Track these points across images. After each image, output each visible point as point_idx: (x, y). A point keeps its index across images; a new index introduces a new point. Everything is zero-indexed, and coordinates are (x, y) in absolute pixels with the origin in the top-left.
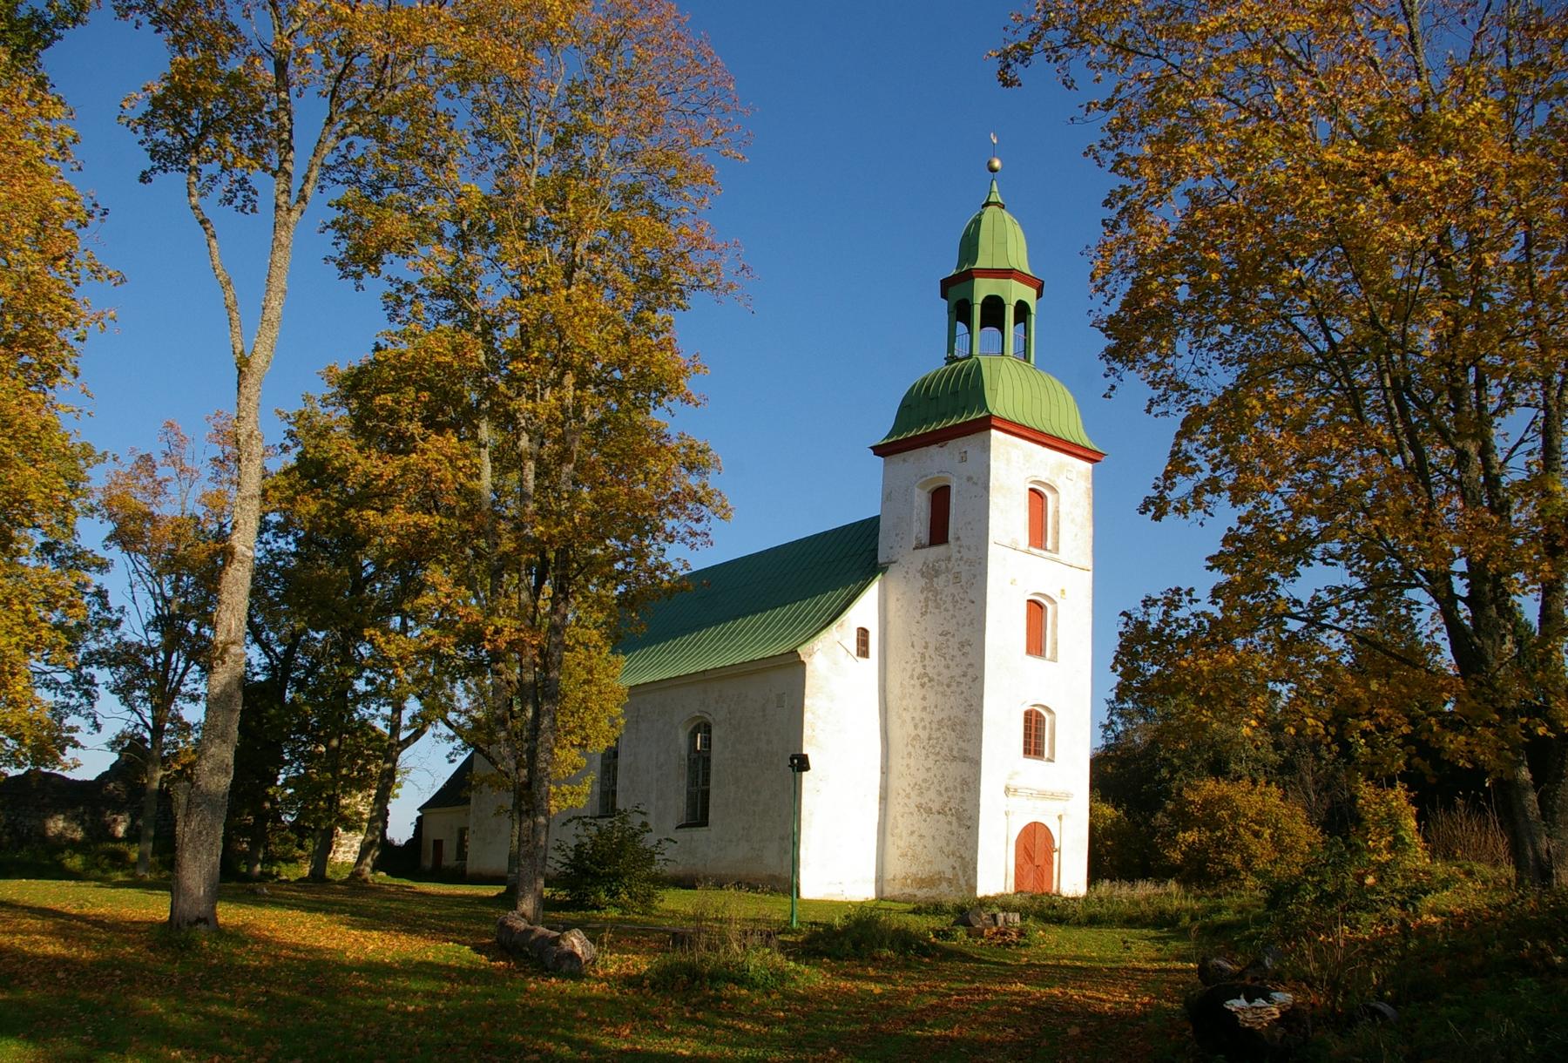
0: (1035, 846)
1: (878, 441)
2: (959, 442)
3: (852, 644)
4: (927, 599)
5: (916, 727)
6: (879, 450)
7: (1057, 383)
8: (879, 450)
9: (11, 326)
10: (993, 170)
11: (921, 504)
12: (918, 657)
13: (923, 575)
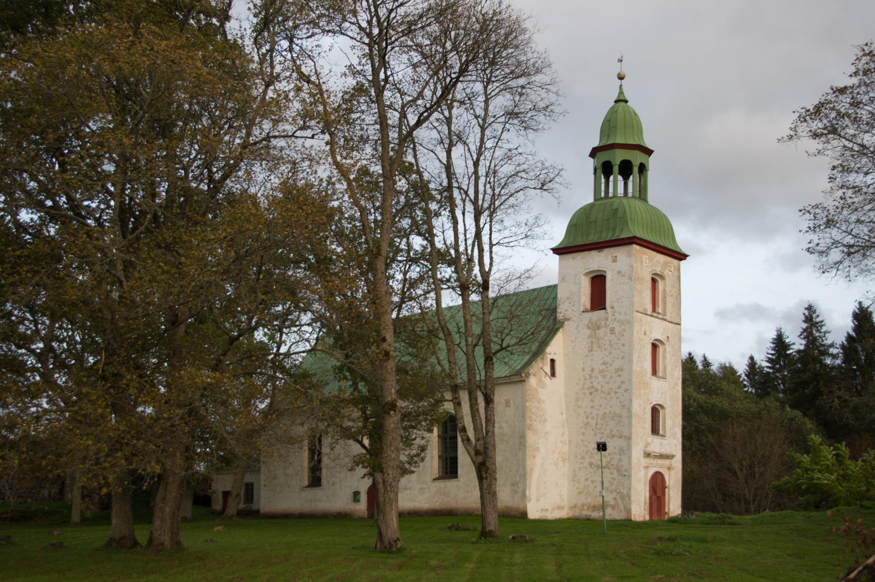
0: (657, 484)
1: (555, 243)
2: (612, 250)
3: (548, 369)
4: (592, 342)
5: (587, 417)
6: (556, 251)
8: (556, 251)
11: (585, 286)
12: (587, 377)
13: (589, 328)
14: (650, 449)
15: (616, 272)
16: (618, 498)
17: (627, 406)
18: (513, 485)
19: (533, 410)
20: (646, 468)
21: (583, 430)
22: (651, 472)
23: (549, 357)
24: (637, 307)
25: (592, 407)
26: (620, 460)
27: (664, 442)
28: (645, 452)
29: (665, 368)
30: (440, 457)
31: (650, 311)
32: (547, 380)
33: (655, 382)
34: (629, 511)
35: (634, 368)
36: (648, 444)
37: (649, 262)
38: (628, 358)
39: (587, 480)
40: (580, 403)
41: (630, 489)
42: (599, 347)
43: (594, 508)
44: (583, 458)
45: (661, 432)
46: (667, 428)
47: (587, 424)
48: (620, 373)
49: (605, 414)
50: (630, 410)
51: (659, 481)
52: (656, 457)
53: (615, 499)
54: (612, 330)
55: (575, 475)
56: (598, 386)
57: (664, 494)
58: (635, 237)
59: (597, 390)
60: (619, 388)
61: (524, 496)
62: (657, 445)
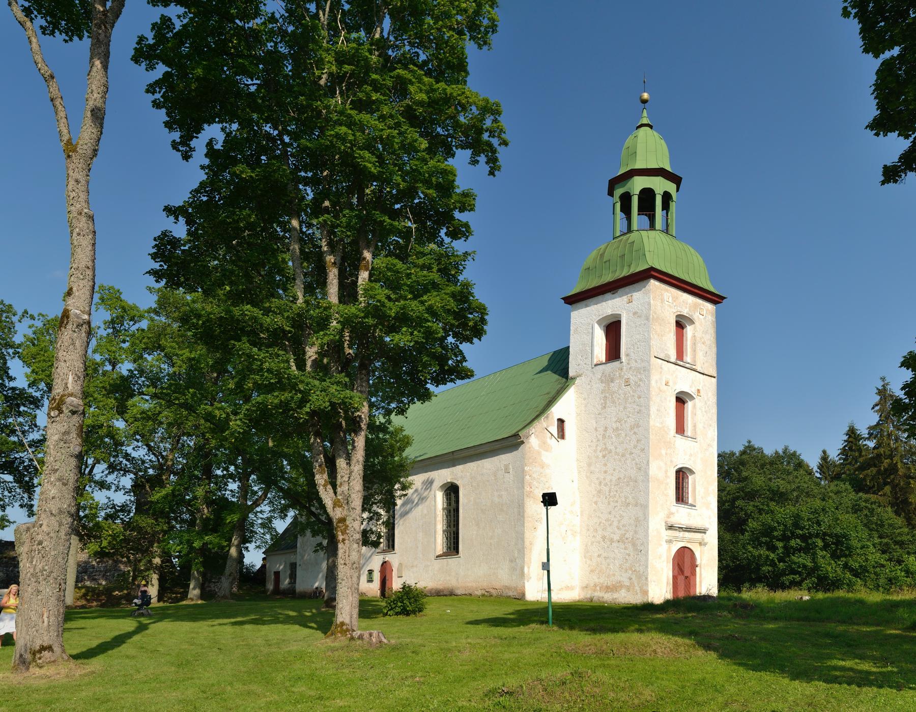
0: (684, 563)
3: (554, 429)
7: (692, 250)
9: (190, 708)
10: (644, 102)
12: (600, 437)
15: (631, 315)
16: (634, 577)
17: (643, 469)
18: (511, 561)
19: (535, 475)
20: (670, 542)
21: (595, 499)
23: (556, 417)
24: (655, 351)
25: (605, 472)
26: (636, 532)
29: (695, 426)
30: (444, 531)
31: (673, 358)
32: (553, 442)
34: (646, 593)
35: (651, 423)
36: (670, 514)
38: (643, 411)
39: (599, 556)
40: (592, 468)
41: (647, 567)
42: (613, 402)
43: (608, 589)
44: (596, 530)
45: (690, 501)
47: (599, 492)
48: (636, 430)
49: (619, 478)
50: (646, 474)
51: (687, 560)
53: (631, 579)
55: (587, 551)
56: (612, 448)
57: (694, 573)
58: (652, 269)
59: (610, 452)
60: (635, 447)
61: (522, 574)
62: (682, 515)
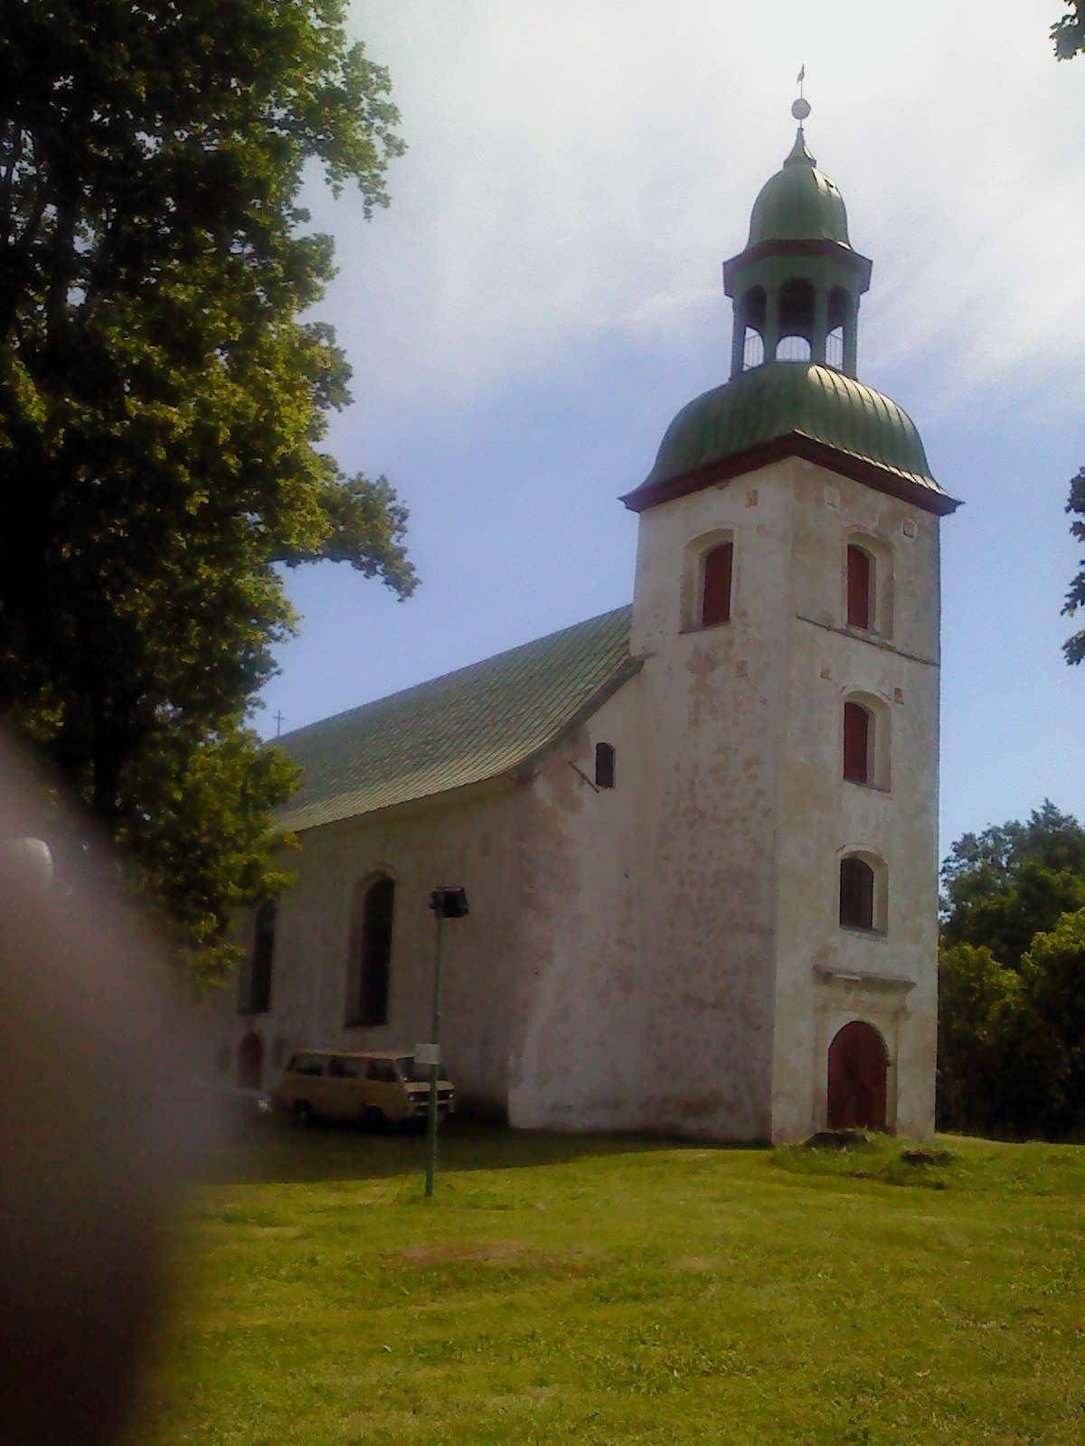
3: (589, 766)
14: (833, 962)
22: (835, 1025)
27: (882, 948)
28: (816, 968)
33: (855, 798)
37: (844, 510)
46: (891, 913)
52: (850, 984)
53: (735, 1087)
54: (741, 668)
60: (752, 807)
